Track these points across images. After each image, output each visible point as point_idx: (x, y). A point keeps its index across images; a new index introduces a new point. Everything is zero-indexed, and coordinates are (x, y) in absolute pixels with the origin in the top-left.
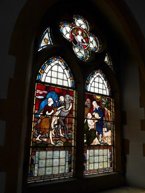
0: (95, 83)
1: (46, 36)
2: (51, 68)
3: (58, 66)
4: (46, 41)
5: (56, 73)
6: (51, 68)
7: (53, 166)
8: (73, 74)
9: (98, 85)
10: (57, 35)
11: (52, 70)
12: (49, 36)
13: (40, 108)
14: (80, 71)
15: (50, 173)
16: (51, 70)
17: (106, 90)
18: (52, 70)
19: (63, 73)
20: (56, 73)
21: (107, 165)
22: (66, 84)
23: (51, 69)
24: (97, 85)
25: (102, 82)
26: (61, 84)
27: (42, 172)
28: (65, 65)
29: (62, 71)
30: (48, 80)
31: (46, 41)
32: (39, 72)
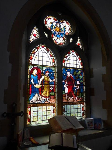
5: (42, 57)
9: (73, 61)
10: (43, 29)
11: (70, 60)
14: (60, 53)
18: (70, 60)
20: (42, 57)
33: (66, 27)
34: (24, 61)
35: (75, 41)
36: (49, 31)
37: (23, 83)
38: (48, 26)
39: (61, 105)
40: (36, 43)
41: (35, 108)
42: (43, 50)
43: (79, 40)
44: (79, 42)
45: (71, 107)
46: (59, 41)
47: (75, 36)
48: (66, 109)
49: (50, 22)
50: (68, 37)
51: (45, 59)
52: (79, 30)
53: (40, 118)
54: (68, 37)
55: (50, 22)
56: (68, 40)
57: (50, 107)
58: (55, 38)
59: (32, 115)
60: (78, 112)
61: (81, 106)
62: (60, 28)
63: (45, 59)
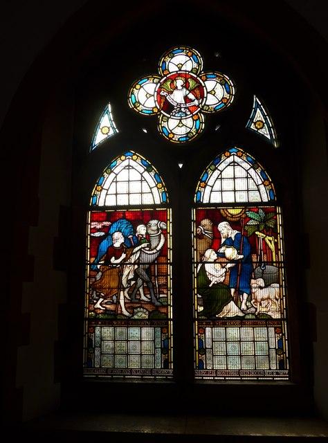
14: (181, 167)
17: (259, 190)
18: (221, 179)
19: (141, 181)
23: (220, 177)
44: (259, 116)
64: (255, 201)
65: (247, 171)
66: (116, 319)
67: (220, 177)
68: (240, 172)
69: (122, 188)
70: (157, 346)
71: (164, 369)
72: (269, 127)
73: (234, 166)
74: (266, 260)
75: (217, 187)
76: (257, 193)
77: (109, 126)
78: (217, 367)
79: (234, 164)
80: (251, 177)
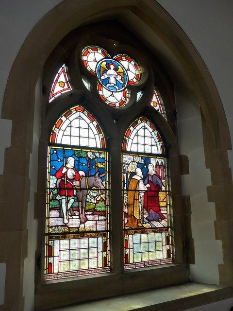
0: (139, 137)
1: (62, 78)
2: (70, 123)
3: (144, 128)
4: (62, 84)
5: (78, 131)
6: (70, 123)
7: (79, 259)
8: (103, 127)
9: (142, 139)
10: (78, 71)
11: (138, 136)
12: (59, 76)
13: (152, 189)
14: (114, 124)
15: (86, 267)
16: (70, 126)
17: (157, 146)
18: (138, 136)
19: (88, 129)
20: (78, 131)
21: (162, 255)
22: (92, 144)
23: (70, 125)
24: (141, 140)
25: (149, 135)
26: (77, 144)
27: (64, 268)
28: (88, 116)
29: (87, 126)
30: (66, 141)
31: (61, 85)
32: (53, 130)
33: (132, 71)
34: (36, 138)
35: (147, 97)
36: (92, 77)
37: (33, 189)
38: (92, 66)
39: (115, 241)
40: (64, 106)
41: (64, 243)
42: (80, 116)
43: (156, 96)
44: (154, 99)
45: (67, 266)
46: (114, 97)
47: (146, 89)
48: (131, 243)
49: (93, 59)
50: (132, 88)
51: (84, 133)
52: (161, 74)
53: (152, 247)
54: (132, 88)
55: (93, 59)
56: (134, 95)
57: (95, 240)
58: (105, 93)
59: (56, 259)
60: (158, 249)
61: (164, 236)
62: (117, 77)
63: (84, 133)
64: (134, 151)
65: (88, 124)
66: (69, 233)
67: (137, 134)
68: (84, 124)
69: (141, 140)
70: (99, 251)
71: (104, 267)
72: (61, 91)
73: (80, 119)
74: (74, 190)
75: (67, 132)
76: (156, 148)
77: (58, 83)
78: (136, 260)
79: (80, 118)
80: (91, 129)
